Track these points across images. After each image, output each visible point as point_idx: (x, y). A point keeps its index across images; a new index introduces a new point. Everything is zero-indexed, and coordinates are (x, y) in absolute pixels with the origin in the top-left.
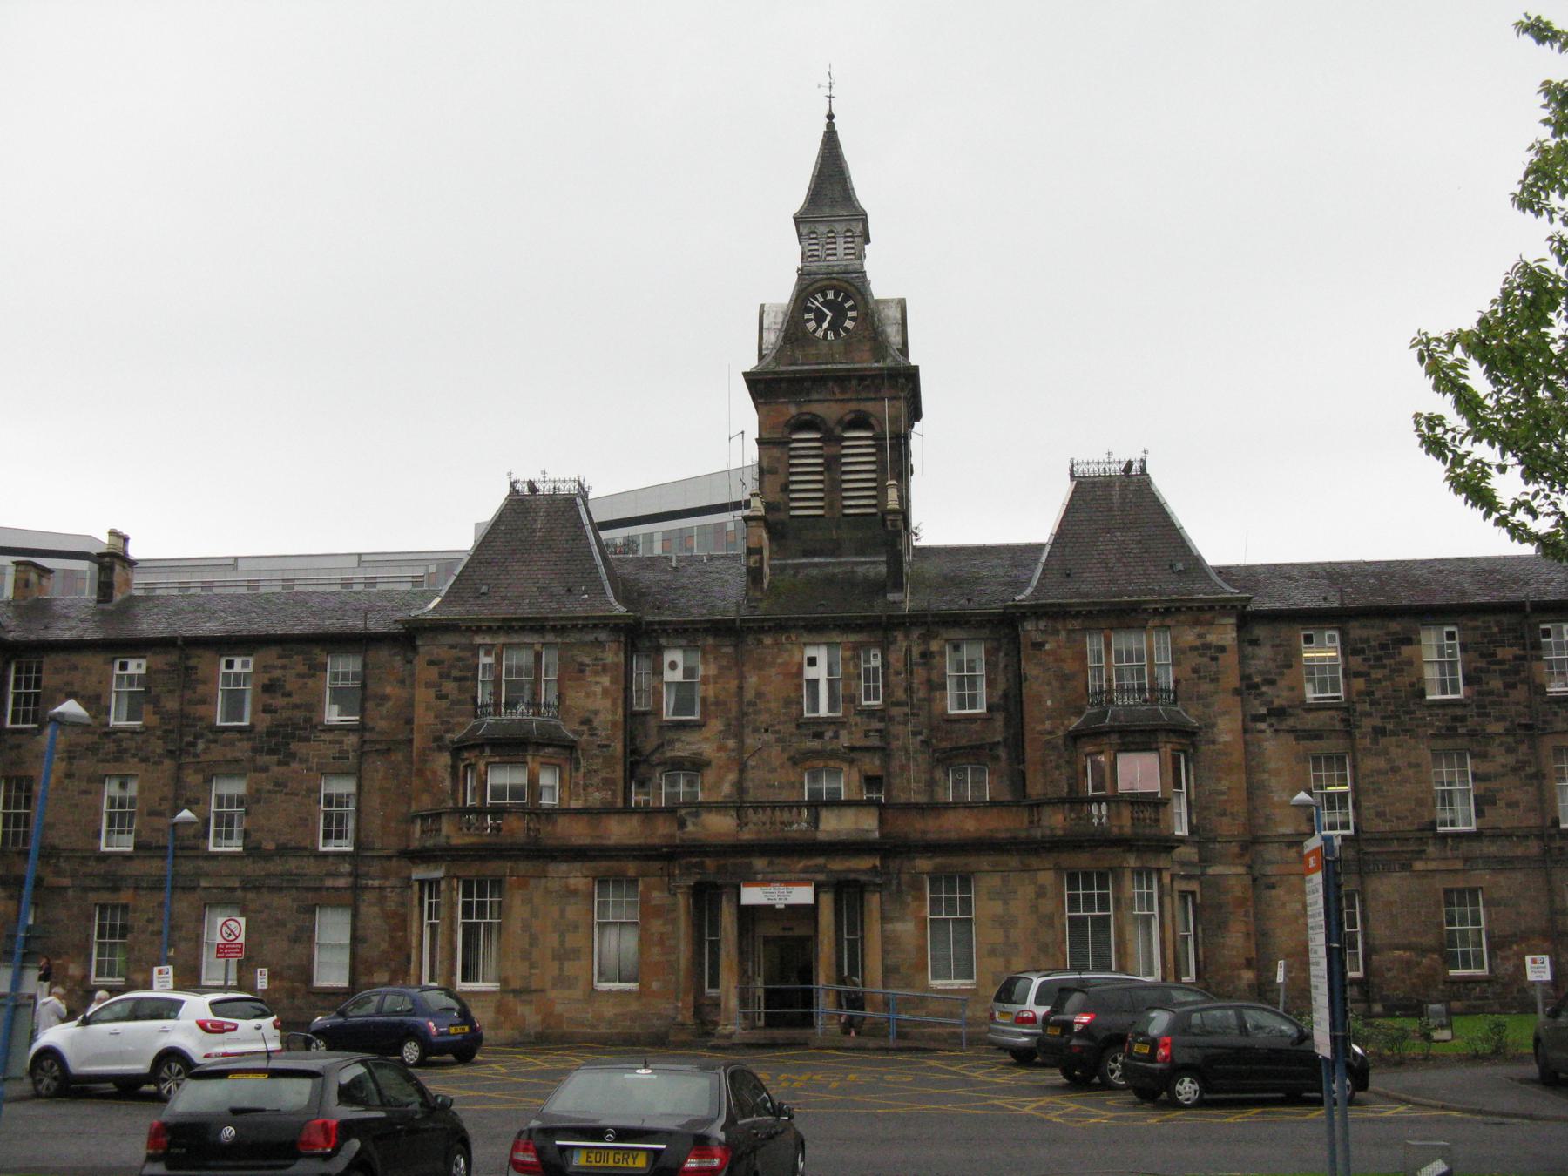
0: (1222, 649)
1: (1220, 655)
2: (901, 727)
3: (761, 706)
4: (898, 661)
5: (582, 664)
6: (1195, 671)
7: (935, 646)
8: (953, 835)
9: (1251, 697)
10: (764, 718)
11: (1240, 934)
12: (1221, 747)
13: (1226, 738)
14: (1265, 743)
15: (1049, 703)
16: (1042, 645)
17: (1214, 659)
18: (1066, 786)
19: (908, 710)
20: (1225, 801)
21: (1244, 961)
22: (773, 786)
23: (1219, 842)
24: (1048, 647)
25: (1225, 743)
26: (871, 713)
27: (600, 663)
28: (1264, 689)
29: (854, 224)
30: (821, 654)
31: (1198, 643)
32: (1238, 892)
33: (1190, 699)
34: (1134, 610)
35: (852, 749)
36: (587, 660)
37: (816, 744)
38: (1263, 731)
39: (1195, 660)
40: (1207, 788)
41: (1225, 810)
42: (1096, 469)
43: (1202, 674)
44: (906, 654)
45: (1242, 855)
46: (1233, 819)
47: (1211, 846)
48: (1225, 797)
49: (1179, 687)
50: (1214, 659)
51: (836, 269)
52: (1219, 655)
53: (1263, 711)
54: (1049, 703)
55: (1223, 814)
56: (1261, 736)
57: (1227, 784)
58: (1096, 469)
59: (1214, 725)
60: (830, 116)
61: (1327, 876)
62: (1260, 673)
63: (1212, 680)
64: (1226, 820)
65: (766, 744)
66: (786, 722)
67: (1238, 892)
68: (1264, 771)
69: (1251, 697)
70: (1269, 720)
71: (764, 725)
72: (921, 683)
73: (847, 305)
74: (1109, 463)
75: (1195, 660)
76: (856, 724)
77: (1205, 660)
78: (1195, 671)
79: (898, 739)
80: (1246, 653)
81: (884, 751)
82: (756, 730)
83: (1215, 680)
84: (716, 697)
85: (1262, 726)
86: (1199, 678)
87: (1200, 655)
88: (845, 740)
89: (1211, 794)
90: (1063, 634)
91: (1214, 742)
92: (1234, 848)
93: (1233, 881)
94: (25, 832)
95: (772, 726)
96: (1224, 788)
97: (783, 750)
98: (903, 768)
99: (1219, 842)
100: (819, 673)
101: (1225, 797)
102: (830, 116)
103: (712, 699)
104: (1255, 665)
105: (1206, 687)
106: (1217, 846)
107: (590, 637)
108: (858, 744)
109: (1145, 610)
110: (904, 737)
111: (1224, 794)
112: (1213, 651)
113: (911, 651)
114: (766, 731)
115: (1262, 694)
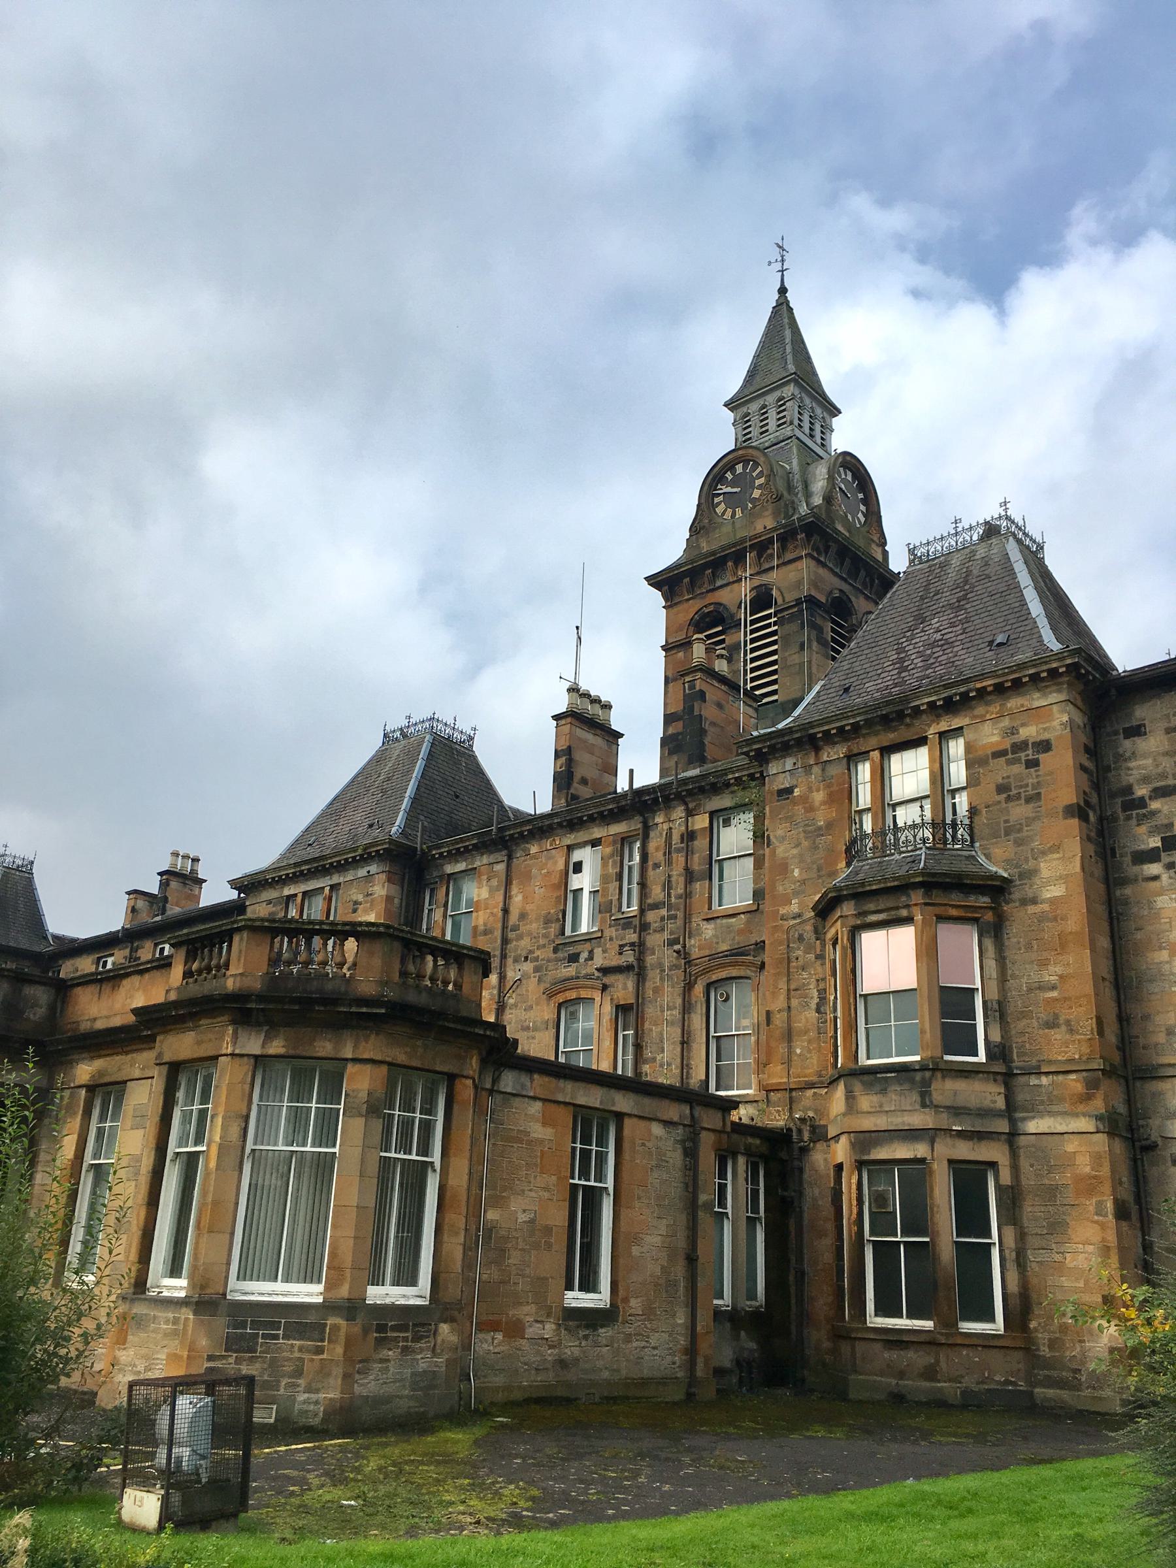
0: (1045, 746)
1: (1042, 757)
2: (658, 935)
3: (523, 929)
4: (657, 849)
5: (356, 903)
6: (1001, 789)
7: (701, 822)
8: (1059, 1119)
9: (1134, 822)
10: (525, 944)
11: (1090, 1248)
12: (1045, 907)
13: (1054, 891)
14: (1159, 898)
15: (796, 873)
16: (789, 791)
17: (1033, 764)
18: (816, 994)
19: (664, 912)
20: (1055, 1000)
21: (1100, 1300)
22: (528, 1028)
23: (1047, 1073)
24: (797, 792)
25: (1053, 901)
26: (626, 923)
27: (369, 898)
28: (1155, 805)
29: (785, 389)
30: (585, 855)
31: (1007, 745)
32: (1084, 1165)
33: (996, 835)
34: (901, 716)
35: (605, 971)
36: (360, 898)
37: (570, 970)
38: (1156, 878)
39: (1001, 771)
40: (1024, 980)
41: (1056, 1016)
42: (939, 548)
43: (1014, 792)
44: (666, 842)
45: (1087, 1098)
46: (1071, 1031)
47: (1034, 1081)
48: (1055, 994)
49: (976, 819)
50: (1033, 764)
51: (767, 444)
52: (1042, 757)
53: (1155, 842)
54: (796, 873)
55: (1052, 1024)
56: (1153, 885)
57: (1059, 969)
58: (939, 548)
59: (1034, 872)
60: (783, 290)
61: (546, 1064)
62: (1145, 780)
63: (1029, 800)
64: (1058, 1035)
65: (526, 976)
66: (544, 946)
67: (1084, 1165)
68: (1161, 948)
69: (1134, 822)
70: (1166, 858)
71: (524, 954)
72: (679, 875)
73: (754, 474)
74: (956, 534)
75: (1001, 771)
76: (611, 939)
77: (1018, 769)
78: (1001, 789)
79: (654, 954)
80: (1121, 750)
81: (638, 971)
82: (516, 961)
83: (1032, 799)
84: (485, 925)
85: (1154, 869)
86: (1009, 799)
87: (1010, 763)
88: (599, 960)
89: (1030, 990)
90: (816, 770)
91: (1034, 901)
92: (1075, 1083)
93: (1071, 1146)
94: (574, 1142)
95: (531, 952)
96: (1054, 979)
97: (540, 980)
98: (656, 990)
99: (1047, 1073)
100: (584, 881)
101: (1055, 994)
102: (783, 290)
103: (482, 928)
104: (1139, 767)
105: (1019, 811)
106: (1044, 1080)
107: (362, 872)
108: (614, 963)
109: (917, 711)
110: (661, 954)
111: (1054, 988)
112: (1030, 752)
113: (671, 833)
114: (526, 958)
115: (1153, 813)
